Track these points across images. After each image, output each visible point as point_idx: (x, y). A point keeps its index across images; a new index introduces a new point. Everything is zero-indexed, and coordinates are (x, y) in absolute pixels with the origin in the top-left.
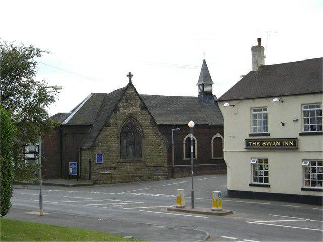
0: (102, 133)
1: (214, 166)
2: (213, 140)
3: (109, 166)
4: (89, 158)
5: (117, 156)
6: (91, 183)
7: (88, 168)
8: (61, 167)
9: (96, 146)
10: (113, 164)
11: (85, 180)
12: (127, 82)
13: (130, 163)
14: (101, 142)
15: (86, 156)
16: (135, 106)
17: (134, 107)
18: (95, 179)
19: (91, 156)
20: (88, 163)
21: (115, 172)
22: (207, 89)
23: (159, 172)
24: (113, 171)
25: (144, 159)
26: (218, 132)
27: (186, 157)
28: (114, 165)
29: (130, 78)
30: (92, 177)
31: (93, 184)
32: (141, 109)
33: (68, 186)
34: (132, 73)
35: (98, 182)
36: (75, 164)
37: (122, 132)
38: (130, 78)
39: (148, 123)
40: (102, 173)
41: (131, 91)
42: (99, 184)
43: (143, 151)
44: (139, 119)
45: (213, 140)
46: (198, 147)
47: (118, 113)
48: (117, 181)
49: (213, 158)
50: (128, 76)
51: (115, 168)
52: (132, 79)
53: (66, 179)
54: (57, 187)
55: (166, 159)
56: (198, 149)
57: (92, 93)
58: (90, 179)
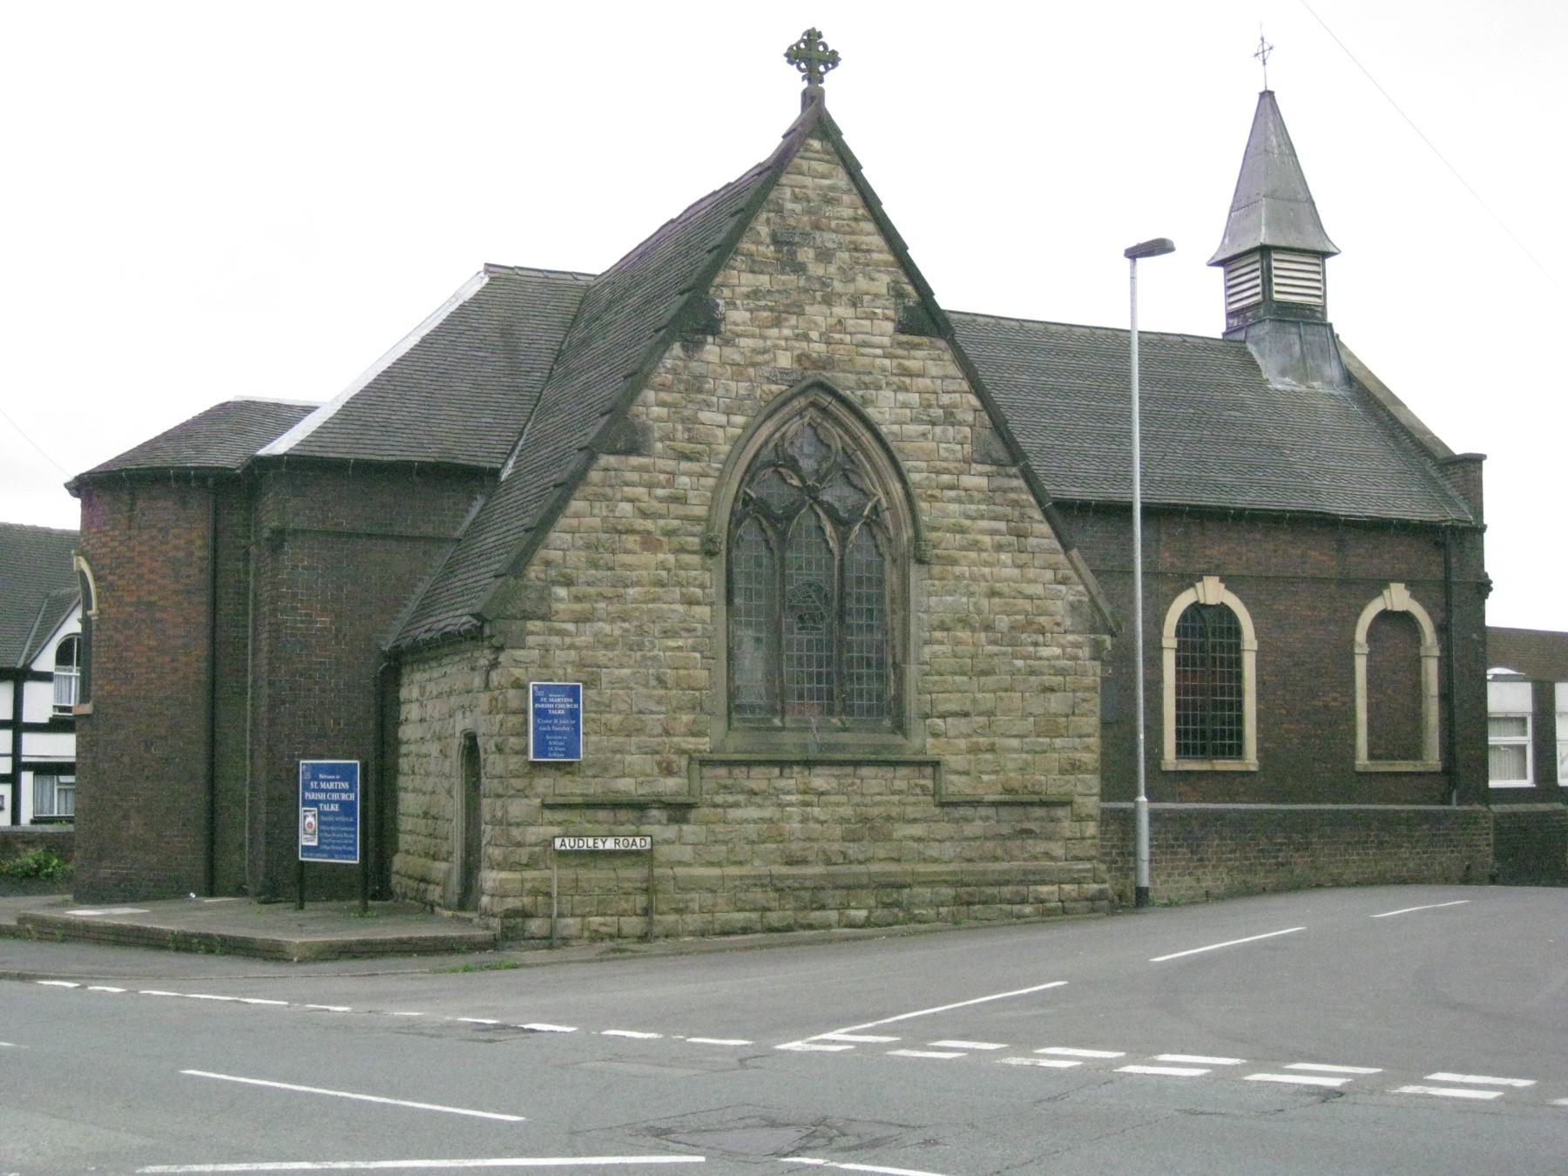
0: (576, 505)
1: (1387, 821)
2: (1361, 635)
3: (626, 785)
4: (462, 723)
5: (696, 707)
6: (479, 934)
7: (453, 807)
8: (212, 766)
9: (527, 617)
10: (668, 770)
11: (428, 907)
12: (791, 112)
13: (808, 764)
14: (568, 582)
15: (435, 709)
16: (855, 302)
17: (841, 310)
18: (511, 903)
19: (484, 699)
20: (454, 763)
21: (680, 839)
22: (1289, 284)
23: (1041, 846)
24: (671, 832)
25: (919, 741)
26: (1397, 579)
27: (1182, 750)
28: (670, 785)
29: (813, 77)
30: (490, 878)
31: (493, 944)
32: (902, 328)
33: (272, 953)
34: (832, 40)
35: (535, 926)
36: (346, 773)
37: (748, 508)
38: (813, 77)
39: (951, 443)
40: (569, 844)
41: (814, 175)
42: (551, 941)
43: (912, 670)
44: (885, 409)
45: (1361, 635)
46: (1261, 683)
47: (711, 351)
48: (694, 920)
49: (1362, 760)
50: (793, 56)
51: (679, 810)
52: (833, 84)
53: (271, 893)
54: (217, 964)
55: (1094, 741)
56: (1260, 696)
57: (489, 268)
58: (468, 895)
